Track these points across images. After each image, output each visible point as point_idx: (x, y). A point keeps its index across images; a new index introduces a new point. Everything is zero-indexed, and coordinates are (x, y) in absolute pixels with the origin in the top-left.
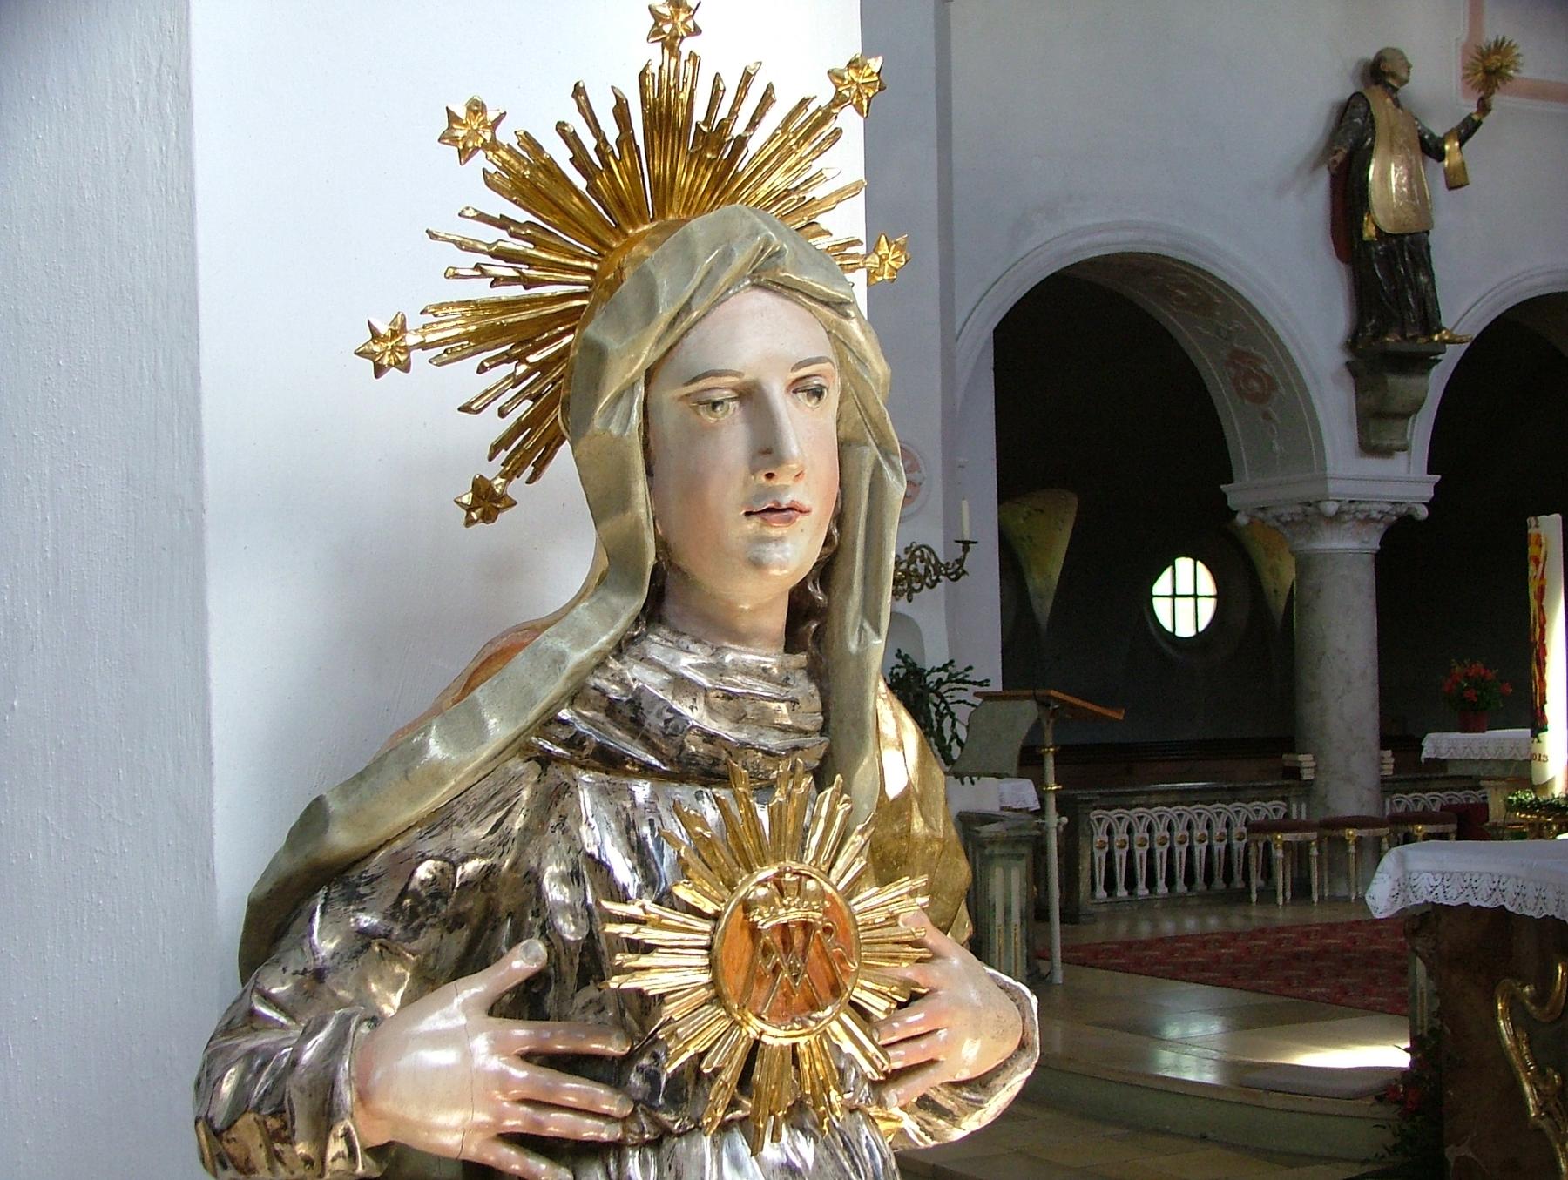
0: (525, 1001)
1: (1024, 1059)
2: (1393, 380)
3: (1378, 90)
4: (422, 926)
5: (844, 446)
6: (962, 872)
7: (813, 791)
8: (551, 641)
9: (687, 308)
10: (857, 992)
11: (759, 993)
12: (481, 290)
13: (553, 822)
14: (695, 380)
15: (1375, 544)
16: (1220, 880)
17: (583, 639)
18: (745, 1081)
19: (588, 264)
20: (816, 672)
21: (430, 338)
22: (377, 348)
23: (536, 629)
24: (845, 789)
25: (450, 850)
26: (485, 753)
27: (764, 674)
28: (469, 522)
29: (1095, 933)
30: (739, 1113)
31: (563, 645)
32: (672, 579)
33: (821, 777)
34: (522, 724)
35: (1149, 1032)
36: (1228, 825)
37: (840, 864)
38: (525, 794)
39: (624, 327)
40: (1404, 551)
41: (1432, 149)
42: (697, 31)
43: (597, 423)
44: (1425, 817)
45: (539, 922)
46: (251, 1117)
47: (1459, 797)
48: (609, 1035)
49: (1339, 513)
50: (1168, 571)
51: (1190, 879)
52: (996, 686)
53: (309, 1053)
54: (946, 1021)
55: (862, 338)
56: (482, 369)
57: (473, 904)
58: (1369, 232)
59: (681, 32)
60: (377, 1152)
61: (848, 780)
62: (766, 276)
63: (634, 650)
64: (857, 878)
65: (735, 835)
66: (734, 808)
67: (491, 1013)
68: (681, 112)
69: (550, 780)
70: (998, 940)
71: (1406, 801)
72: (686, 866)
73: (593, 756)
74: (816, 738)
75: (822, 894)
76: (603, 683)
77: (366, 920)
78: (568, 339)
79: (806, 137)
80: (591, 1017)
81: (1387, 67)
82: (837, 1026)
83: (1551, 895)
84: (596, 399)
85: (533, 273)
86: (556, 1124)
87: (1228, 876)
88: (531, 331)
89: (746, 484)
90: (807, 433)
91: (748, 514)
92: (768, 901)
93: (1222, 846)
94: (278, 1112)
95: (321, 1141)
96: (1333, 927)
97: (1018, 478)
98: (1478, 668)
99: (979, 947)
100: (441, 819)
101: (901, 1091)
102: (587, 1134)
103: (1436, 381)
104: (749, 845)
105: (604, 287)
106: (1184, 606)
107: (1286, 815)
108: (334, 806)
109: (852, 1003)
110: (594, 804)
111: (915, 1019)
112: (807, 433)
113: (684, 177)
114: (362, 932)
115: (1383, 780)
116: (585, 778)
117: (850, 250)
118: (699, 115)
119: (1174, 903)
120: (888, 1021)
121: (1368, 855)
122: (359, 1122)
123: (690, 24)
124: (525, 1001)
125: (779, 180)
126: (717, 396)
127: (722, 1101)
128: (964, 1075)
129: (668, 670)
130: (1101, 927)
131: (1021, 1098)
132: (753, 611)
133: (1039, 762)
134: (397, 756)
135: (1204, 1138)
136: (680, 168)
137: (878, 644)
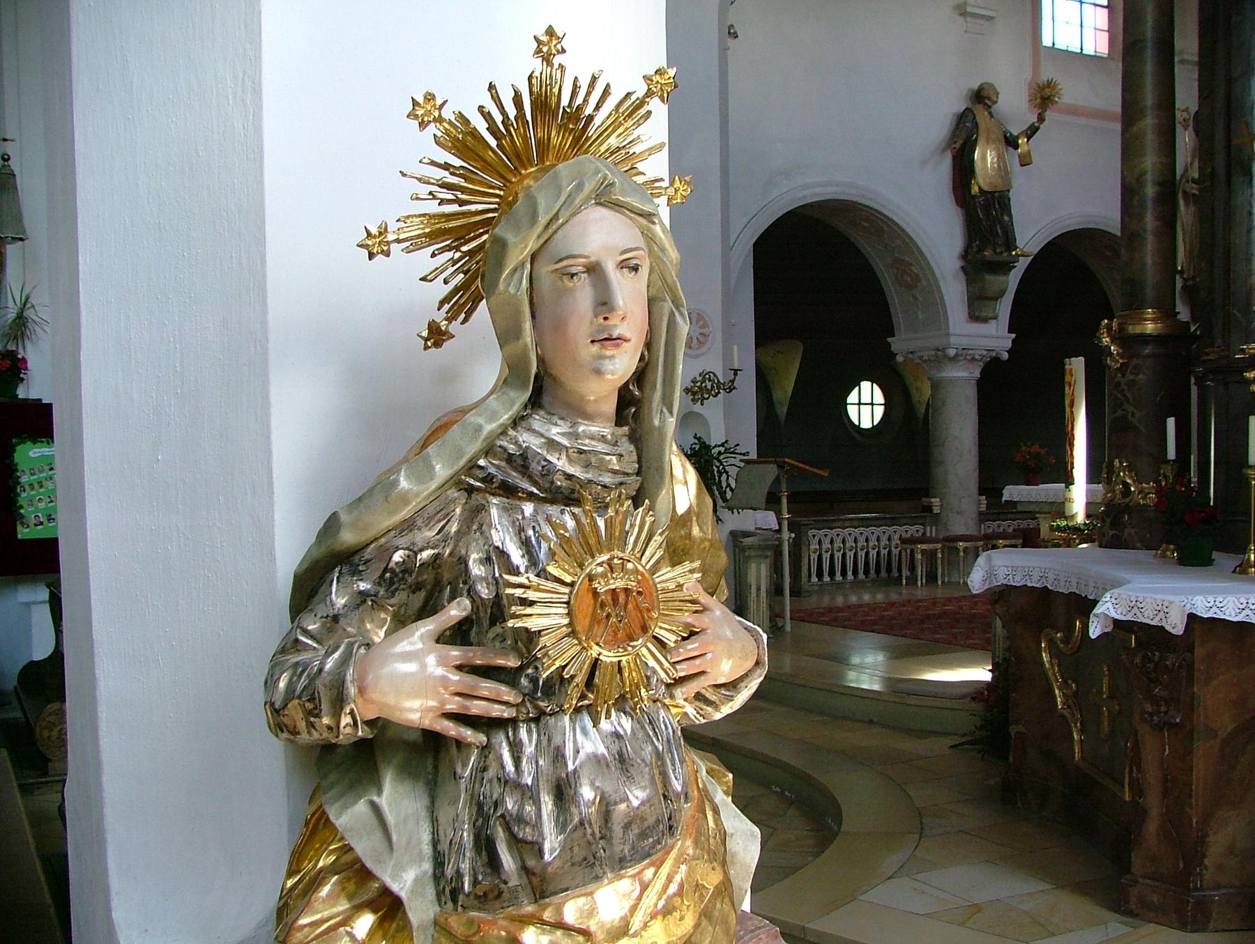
0: (459, 634)
1: (759, 671)
2: (988, 277)
3: (980, 107)
4: (397, 589)
5: (651, 302)
6: (723, 560)
7: (631, 509)
8: (472, 418)
9: (556, 217)
10: (657, 630)
11: (598, 630)
12: (433, 207)
13: (475, 527)
14: (561, 260)
15: (977, 374)
16: (884, 572)
17: (493, 417)
18: (589, 683)
19: (497, 192)
20: (634, 438)
21: (402, 236)
22: (370, 243)
23: (464, 411)
24: (651, 508)
25: (413, 544)
26: (434, 485)
27: (603, 439)
28: (426, 348)
29: (811, 602)
30: (586, 702)
31: (481, 421)
32: (547, 383)
33: (637, 501)
34: (456, 468)
35: (841, 660)
36: (889, 539)
37: (648, 553)
38: (458, 511)
39: (517, 228)
40: (995, 380)
41: (1011, 142)
42: (563, 51)
43: (501, 287)
44: (1004, 536)
45: (467, 587)
46: (296, 702)
47: (1024, 524)
48: (508, 655)
49: (957, 355)
50: (857, 389)
51: (866, 572)
52: (753, 456)
53: (330, 664)
54: (712, 648)
55: (663, 236)
56: (433, 255)
57: (427, 577)
58: (975, 190)
59: (554, 51)
60: (370, 723)
61: (653, 502)
62: (604, 198)
63: (524, 424)
64: (658, 562)
65: (584, 536)
66: (583, 519)
67: (438, 641)
68: (554, 100)
69: (473, 502)
70: (752, 606)
71: (993, 527)
72: (554, 554)
73: (499, 488)
74: (634, 477)
75: (637, 571)
76: (504, 443)
77: (363, 586)
78: (485, 237)
79: (630, 115)
80: (498, 644)
81: (985, 93)
82: (645, 650)
83: (1074, 580)
84: (501, 273)
85: (464, 197)
86: (477, 708)
87: (889, 570)
88: (463, 233)
89: (591, 323)
90: (629, 293)
91: (592, 342)
92: (603, 575)
93: (886, 552)
94: (312, 699)
95: (337, 715)
96: (949, 600)
97: (765, 335)
98: (1036, 448)
99: (739, 607)
100: (408, 526)
101: (684, 690)
102: (494, 714)
103: (1013, 279)
104: (592, 541)
105: (506, 205)
106: (866, 410)
107: (924, 534)
108: (344, 517)
109: (654, 637)
110: (500, 517)
111: (693, 647)
112: (629, 293)
113: (555, 140)
114: (361, 593)
115: (981, 513)
116: (494, 501)
117: (657, 184)
118: (565, 101)
119: (857, 585)
120: (676, 648)
121: (970, 557)
122: (360, 705)
123: (559, 47)
124: (459, 634)
125: (613, 141)
126: (574, 270)
127: (576, 695)
128: (722, 680)
129: (545, 437)
130: (814, 598)
131: (755, 696)
132: (595, 401)
133: (779, 501)
134: (383, 486)
135: (871, 722)
136: (553, 133)
137: (672, 422)
